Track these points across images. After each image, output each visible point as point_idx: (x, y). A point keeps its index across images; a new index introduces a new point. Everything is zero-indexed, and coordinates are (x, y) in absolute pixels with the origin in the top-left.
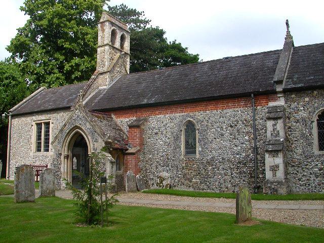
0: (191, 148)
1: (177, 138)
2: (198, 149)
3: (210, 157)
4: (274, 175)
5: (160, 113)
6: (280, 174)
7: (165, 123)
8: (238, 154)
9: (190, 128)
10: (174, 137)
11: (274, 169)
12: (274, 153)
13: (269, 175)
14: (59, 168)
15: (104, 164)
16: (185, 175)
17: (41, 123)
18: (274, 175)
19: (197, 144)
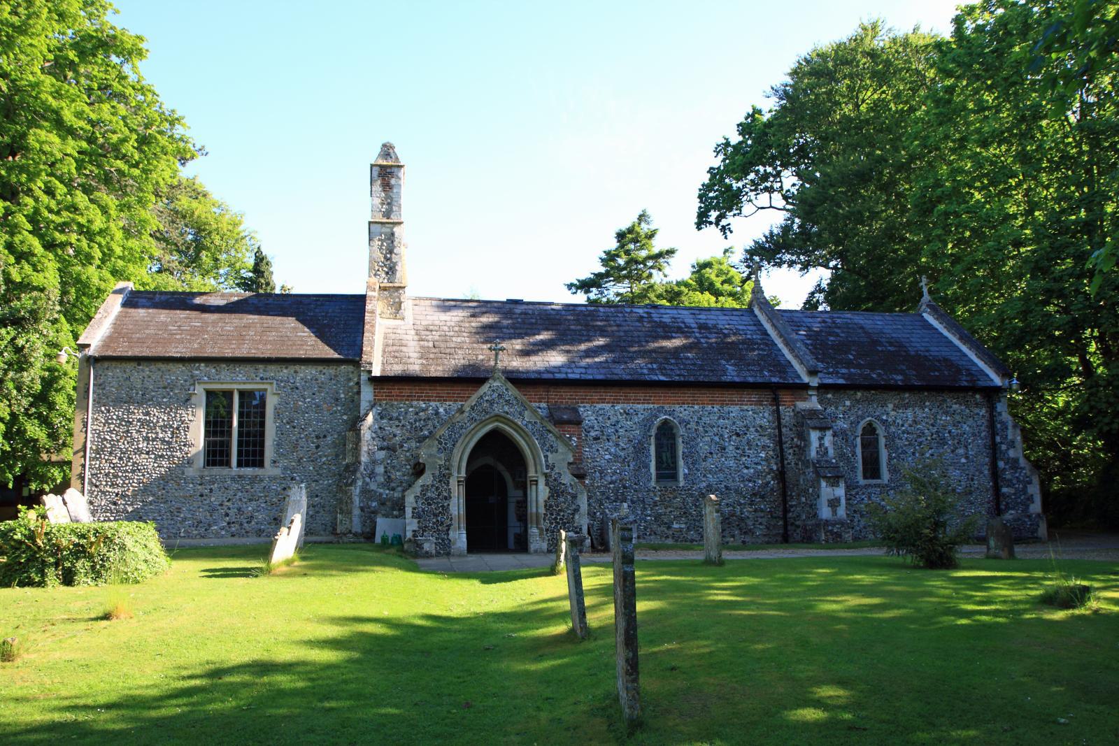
0: (667, 470)
1: (640, 449)
2: (682, 470)
3: (704, 484)
4: (835, 513)
5: (603, 401)
6: (842, 512)
7: (613, 419)
8: (750, 481)
9: (666, 434)
10: (635, 448)
11: (834, 503)
12: (834, 481)
13: (825, 513)
14: (446, 509)
15: (574, 497)
16: (658, 517)
17: (228, 394)
18: (835, 513)
19: (681, 463)
